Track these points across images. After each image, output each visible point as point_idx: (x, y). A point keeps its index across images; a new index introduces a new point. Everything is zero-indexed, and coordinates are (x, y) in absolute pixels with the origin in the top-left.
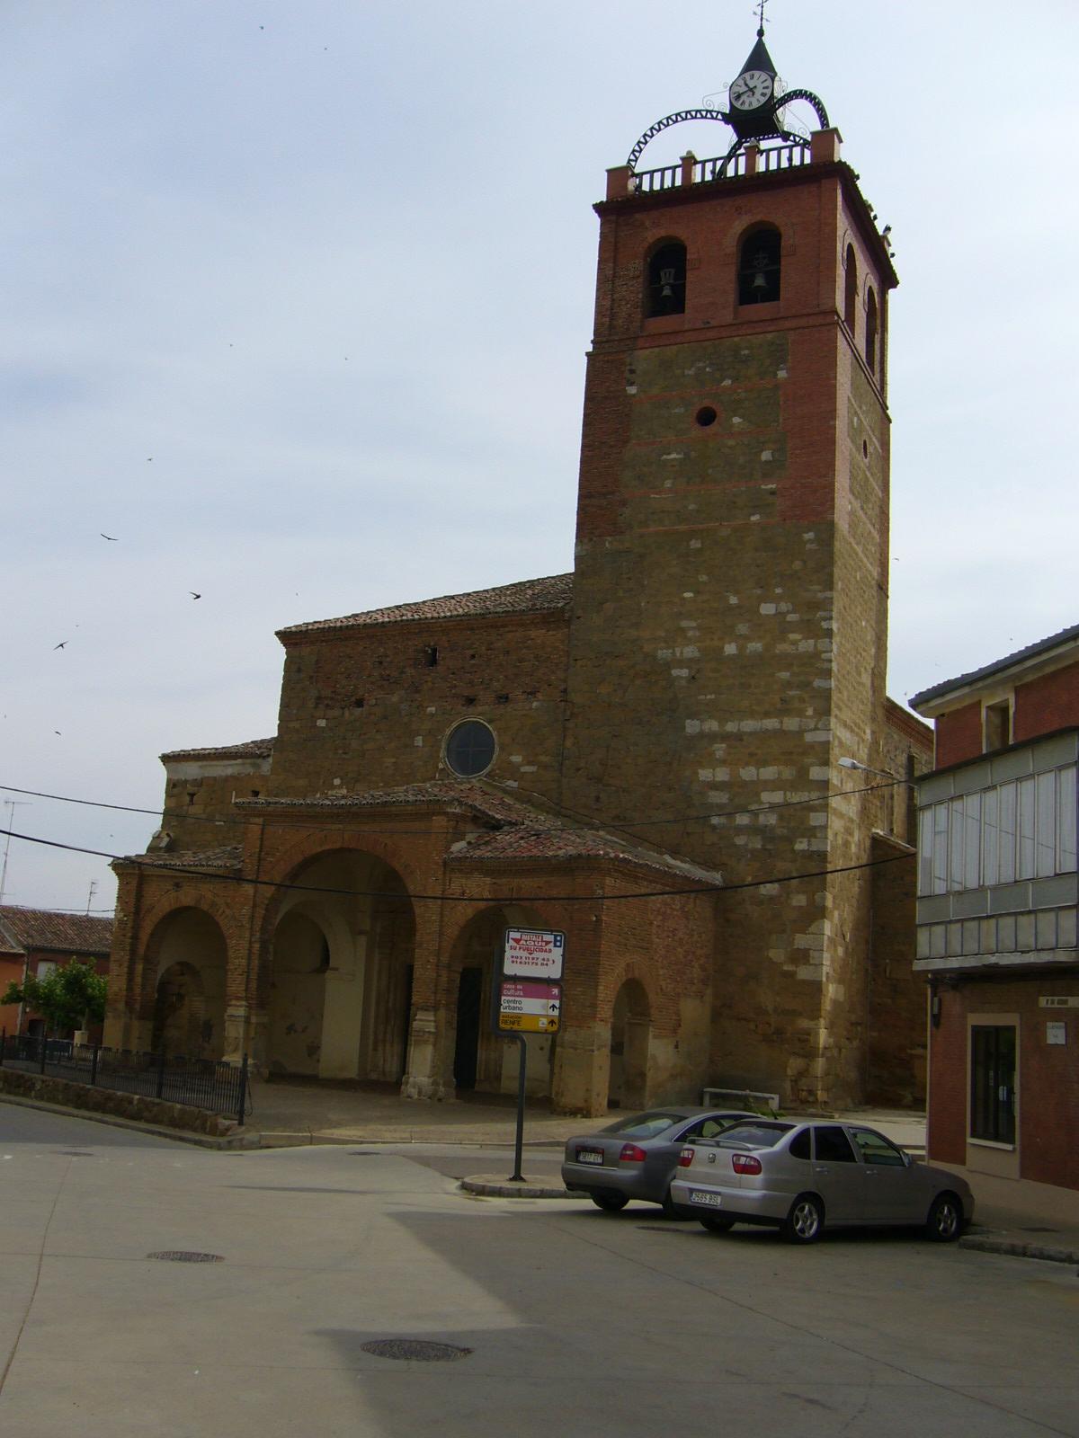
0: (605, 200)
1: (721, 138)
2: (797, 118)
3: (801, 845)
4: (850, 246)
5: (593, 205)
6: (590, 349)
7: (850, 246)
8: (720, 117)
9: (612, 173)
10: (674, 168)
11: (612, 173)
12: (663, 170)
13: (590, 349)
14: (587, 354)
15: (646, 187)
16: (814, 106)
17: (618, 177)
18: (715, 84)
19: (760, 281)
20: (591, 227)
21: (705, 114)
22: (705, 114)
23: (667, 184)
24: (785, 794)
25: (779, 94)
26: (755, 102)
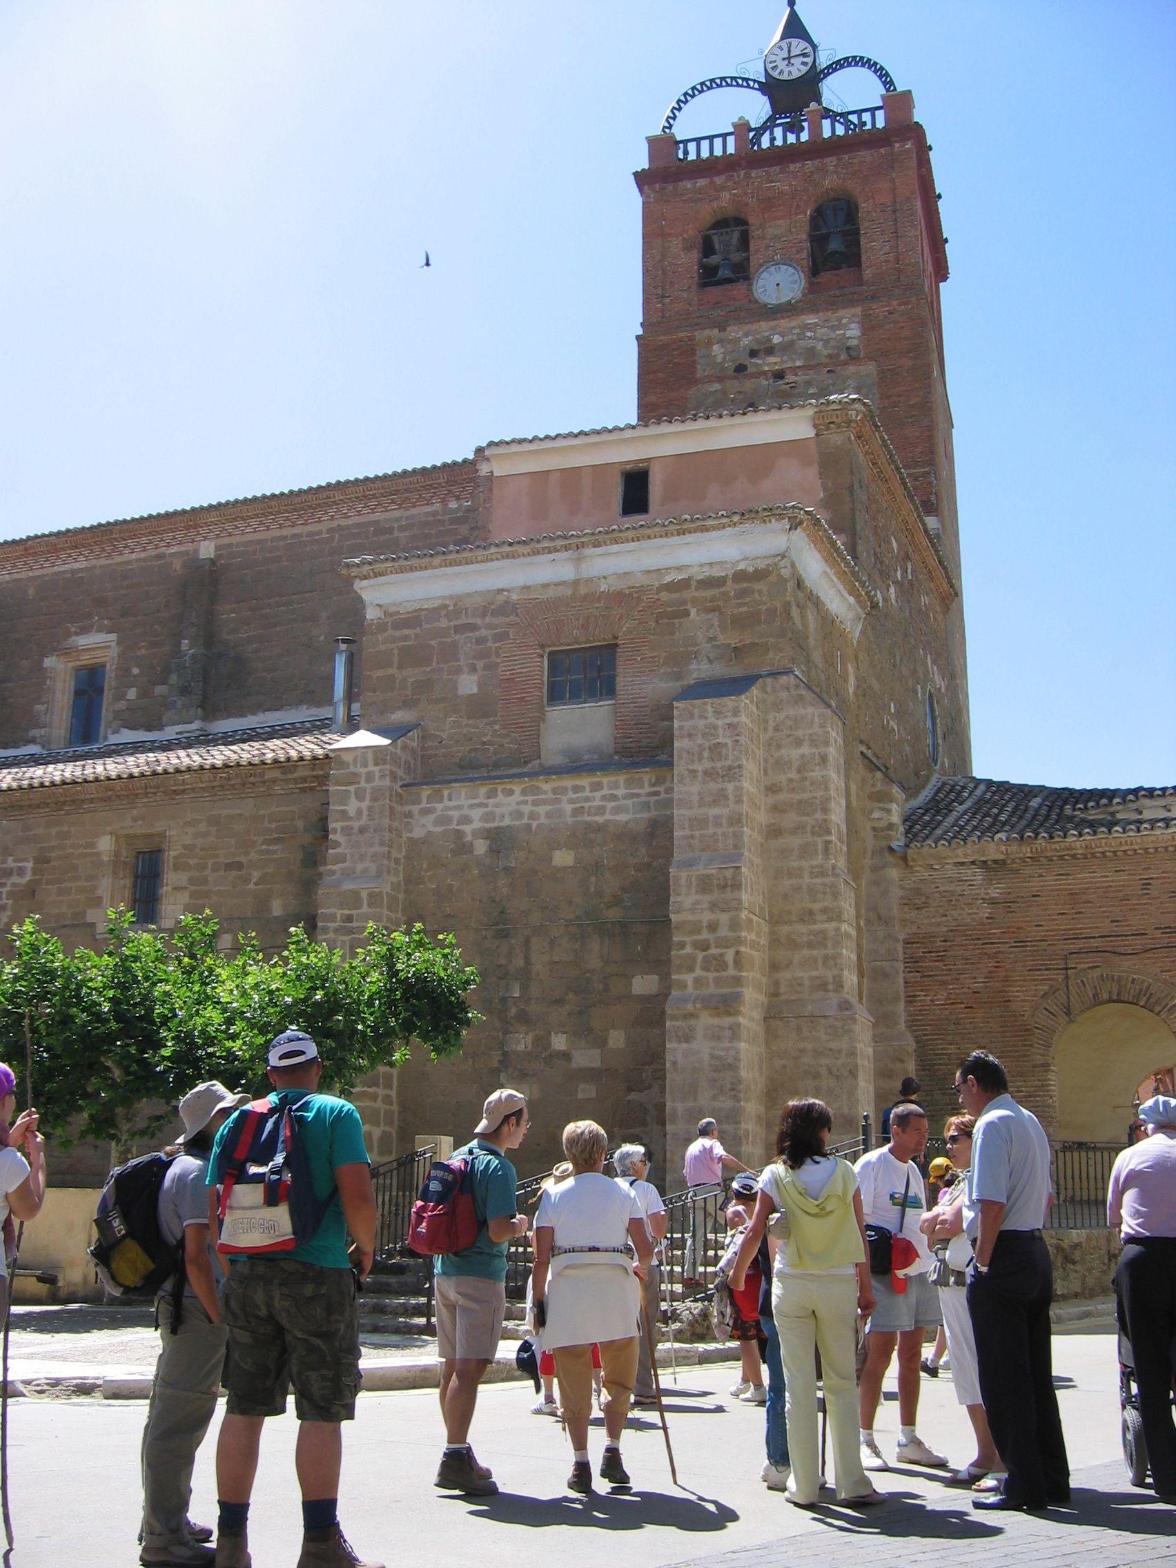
0: (647, 167)
1: (756, 108)
2: (850, 93)
3: (876, 685)
4: (302, 1053)
5: (910, 91)
6: (640, 332)
7: (302, 1053)
8: (756, 86)
9: (652, 141)
10: (724, 136)
11: (652, 141)
12: (711, 138)
13: (640, 332)
14: (638, 337)
15: (692, 156)
16: (880, 77)
17: (663, 146)
18: (756, 44)
19: (835, 245)
20: (630, 206)
21: (744, 83)
22: (744, 83)
23: (705, 154)
24: (667, 1364)
25: (823, 62)
26: (797, 70)
